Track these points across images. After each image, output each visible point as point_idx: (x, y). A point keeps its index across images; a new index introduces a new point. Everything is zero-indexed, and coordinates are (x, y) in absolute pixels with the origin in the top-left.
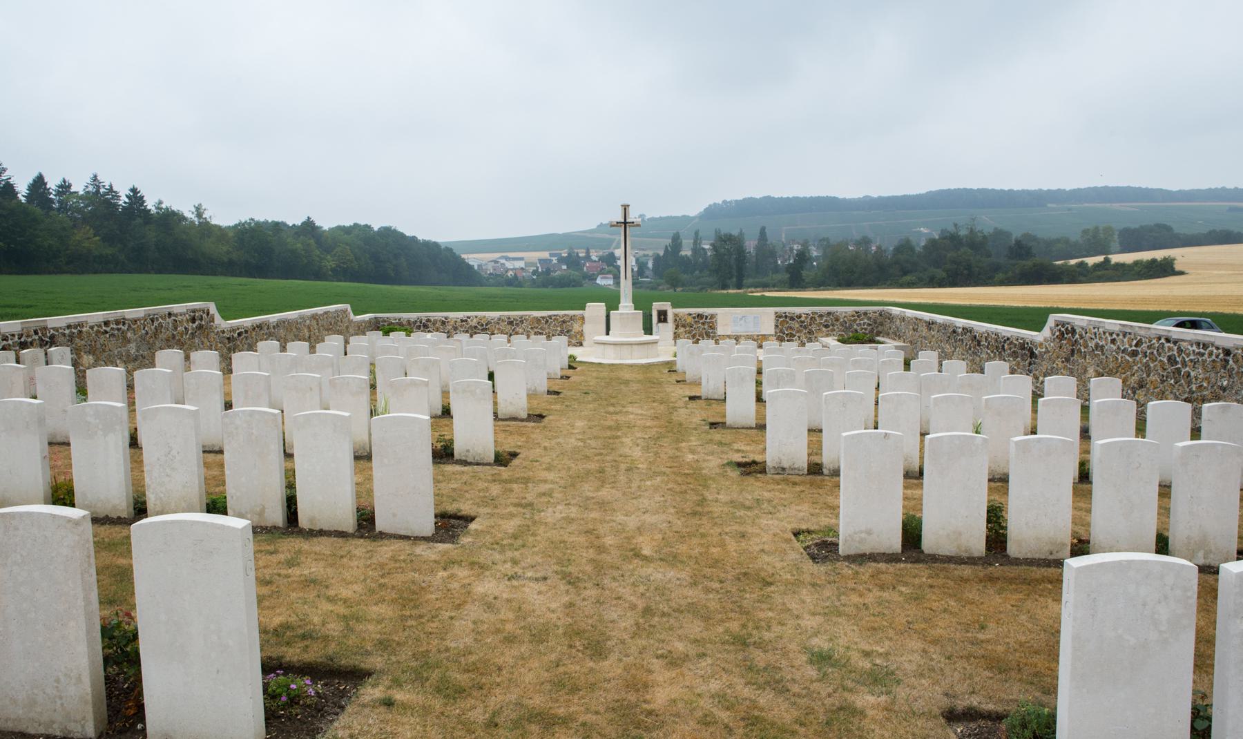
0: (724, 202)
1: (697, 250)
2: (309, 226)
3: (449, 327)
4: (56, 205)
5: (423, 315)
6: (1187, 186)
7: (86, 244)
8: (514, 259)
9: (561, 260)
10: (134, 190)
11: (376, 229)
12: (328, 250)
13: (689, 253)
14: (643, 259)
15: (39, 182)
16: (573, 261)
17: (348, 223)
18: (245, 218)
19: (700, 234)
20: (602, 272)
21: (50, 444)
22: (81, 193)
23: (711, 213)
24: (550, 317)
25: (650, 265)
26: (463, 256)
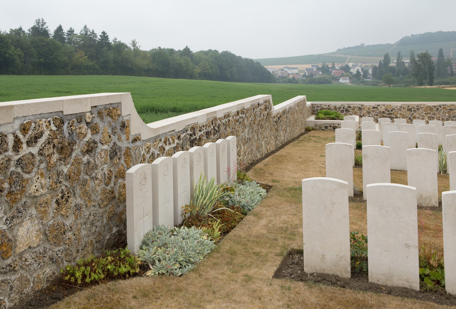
1: (400, 63)
2: (187, 51)
3: (364, 112)
4: (67, 41)
5: (346, 103)
6: (174, 40)
7: (81, 60)
8: (292, 68)
9: (318, 69)
10: (104, 33)
11: (220, 52)
12: (196, 63)
13: (395, 65)
15: (60, 29)
16: (325, 70)
17: (206, 49)
18: (156, 47)
19: (401, 54)
20: (342, 75)
22: (79, 34)
23: (404, 42)
24: (440, 106)
25: (370, 71)
26: (265, 67)
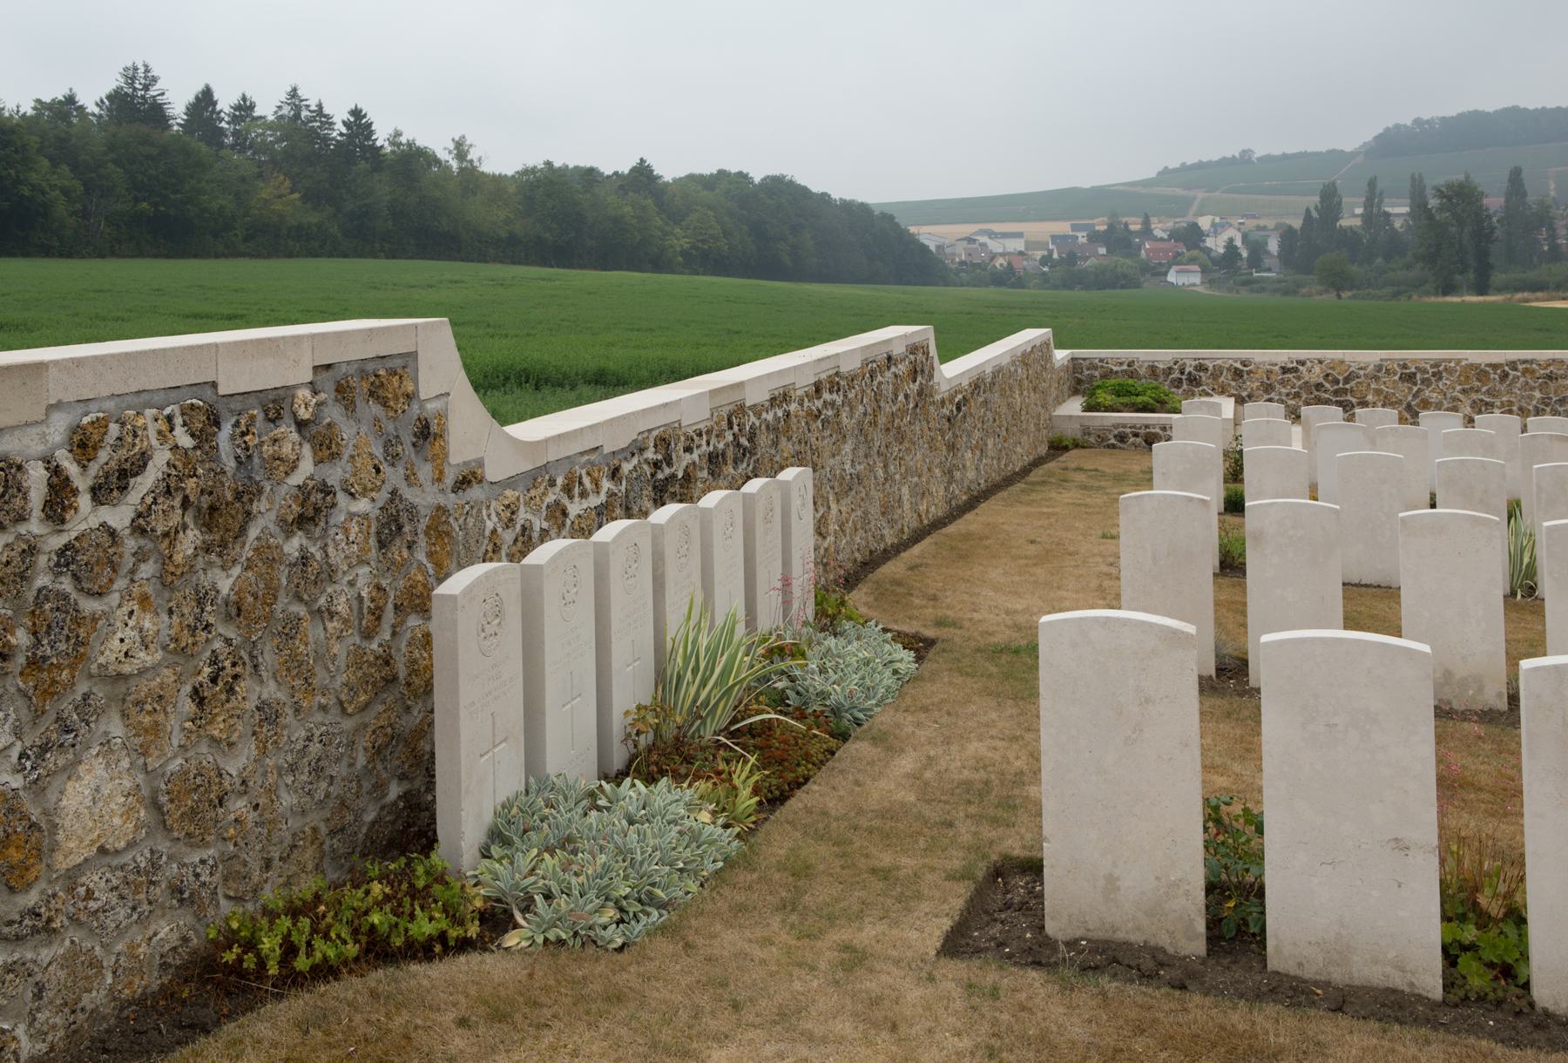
0: (1418, 121)
1: (1376, 217)
4: (229, 140)
5: (1189, 356)
7: (278, 206)
8: (1005, 235)
9: (1094, 237)
10: (357, 113)
11: (757, 180)
14: (1257, 235)
15: (206, 99)
16: (1118, 239)
17: (708, 168)
18: (536, 160)
19: (1380, 185)
20: (1177, 260)
21: (1443, 713)
22: (271, 118)
23: (1390, 144)
24: (1513, 365)
25: (1273, 246)
26: (913, 230)
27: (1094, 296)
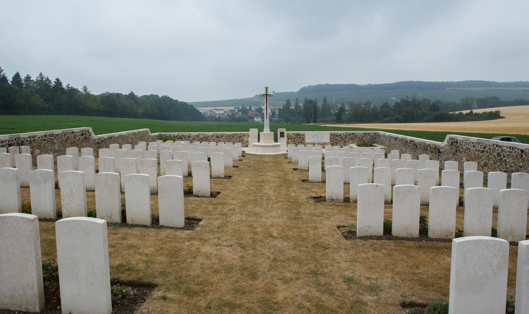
0: (309, 86)
1: (297, 106)
2: (132, 95)
4: (24, 86)
5: (180, 133)
7: (37, 102)
9: (239, 110)
10: (57, 79)
13: (294, 108)
15: (17, 76)
17: (148, 94)
18: (104, 92)
20: (256, 116)
22: (35, 80)
23: (303, 90)
24: (234, 134)
25: (277, 113)
27: (238, 123)
